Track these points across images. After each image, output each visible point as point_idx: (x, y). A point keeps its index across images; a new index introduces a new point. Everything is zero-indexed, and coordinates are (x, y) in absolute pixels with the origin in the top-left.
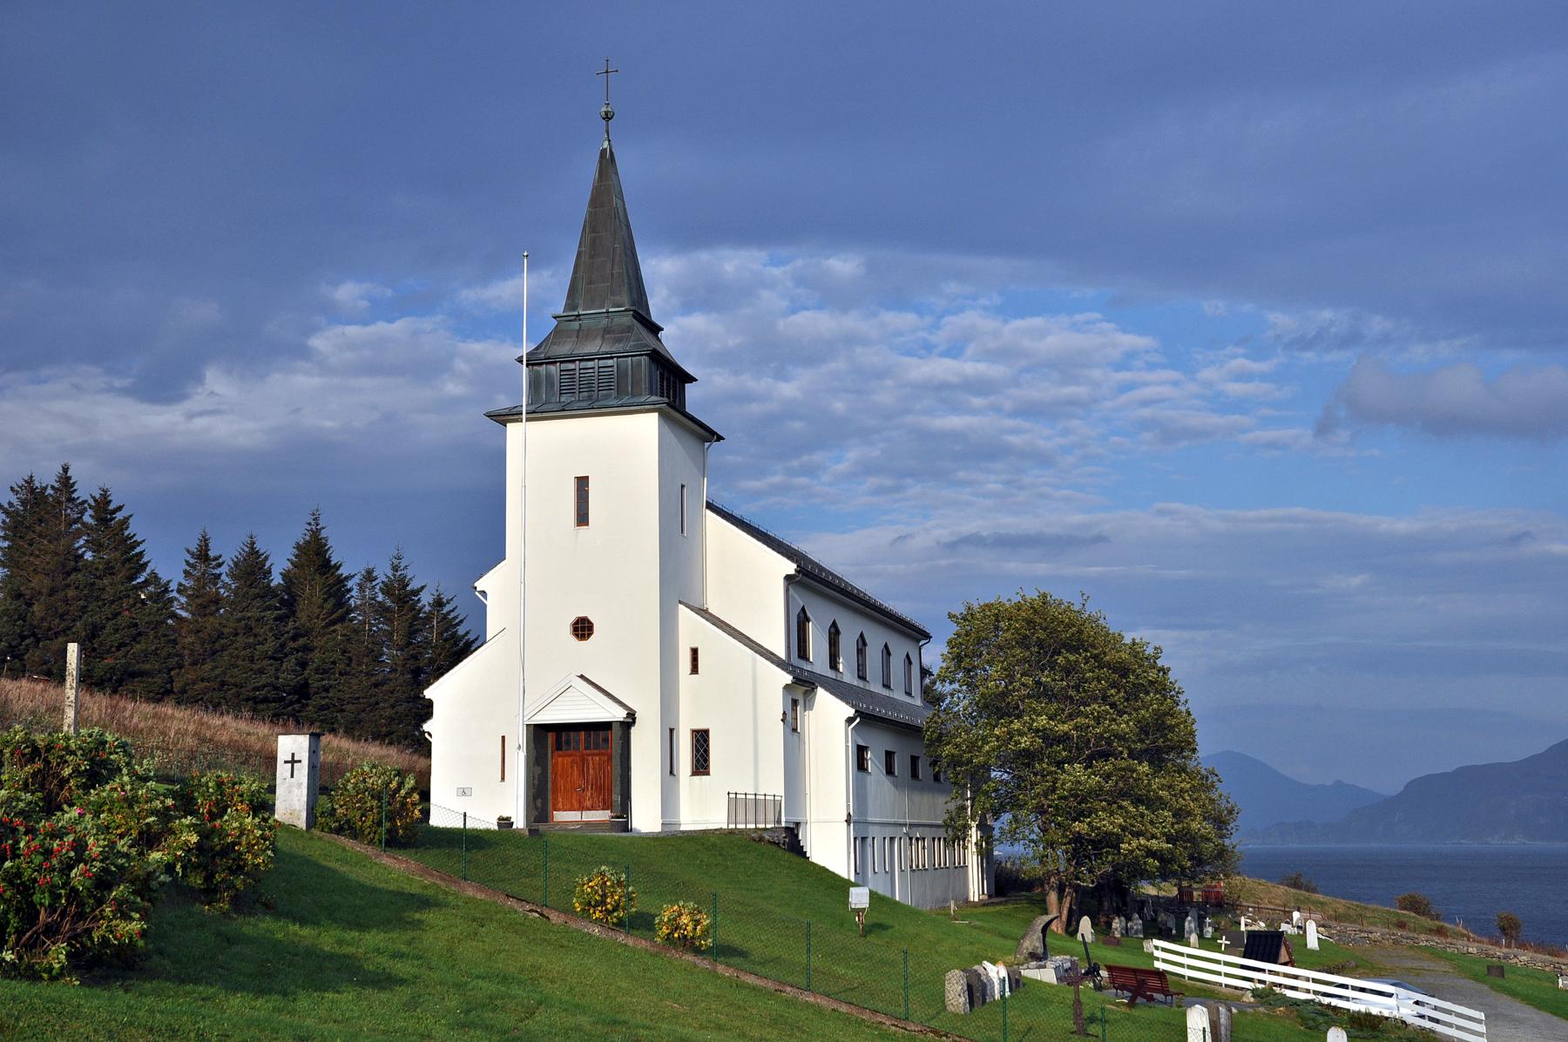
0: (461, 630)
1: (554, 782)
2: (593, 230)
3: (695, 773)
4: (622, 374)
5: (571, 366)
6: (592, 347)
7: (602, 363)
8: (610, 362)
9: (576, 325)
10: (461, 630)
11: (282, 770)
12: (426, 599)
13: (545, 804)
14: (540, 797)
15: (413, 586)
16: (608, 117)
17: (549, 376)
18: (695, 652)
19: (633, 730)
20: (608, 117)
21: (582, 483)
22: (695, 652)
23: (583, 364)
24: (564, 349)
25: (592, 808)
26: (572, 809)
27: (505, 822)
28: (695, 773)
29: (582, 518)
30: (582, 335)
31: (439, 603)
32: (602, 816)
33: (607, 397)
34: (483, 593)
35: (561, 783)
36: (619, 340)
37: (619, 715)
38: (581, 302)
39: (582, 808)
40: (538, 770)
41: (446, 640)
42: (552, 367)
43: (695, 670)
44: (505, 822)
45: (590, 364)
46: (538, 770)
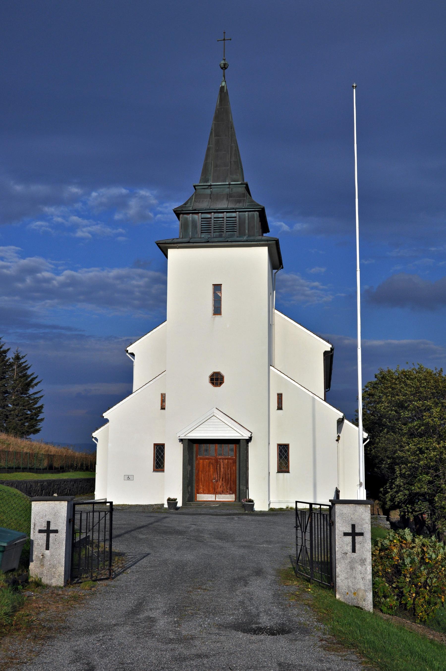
0: (29, 372)
1: (198, 475)
2: (216, 135)
3: (280, 470)
4: (242, 222)
5: (208, 216)
6: (223, 204)
7: (229, 215)
8: (234, 215)
9: (208, 191)
10: (29, 372)
11: (342, 544)
12: (10, 356)
13: (192, 489)
14: (190, 485)
15: (5, 348)
16: (224, 67)
17: (194, 221)
18: (280, 396)
19: (250, 444)
20: (224, 67)
21: (217, 288)
22: (280, 396)
23: (216, 215)
24: (204, 205)
25: (222, 493)
26: (209, 493)
27: (172, 502)
28: (280, 470)
29: (217, 311)
30: (213, 197)
31: (18, 358)
32: (229, 498)
33: (232, 236)
34: (133, 355)
35: (202, 476)
36: (239, 202)
37: (246, 435)
38: (211, 178)
39: (215, 492)
40: (189, 468)
41: (20, 377)
42: (196, 216)
43: (280, 408)
44: (172, 502)
45: (221, 215)
46: (189, 468)
